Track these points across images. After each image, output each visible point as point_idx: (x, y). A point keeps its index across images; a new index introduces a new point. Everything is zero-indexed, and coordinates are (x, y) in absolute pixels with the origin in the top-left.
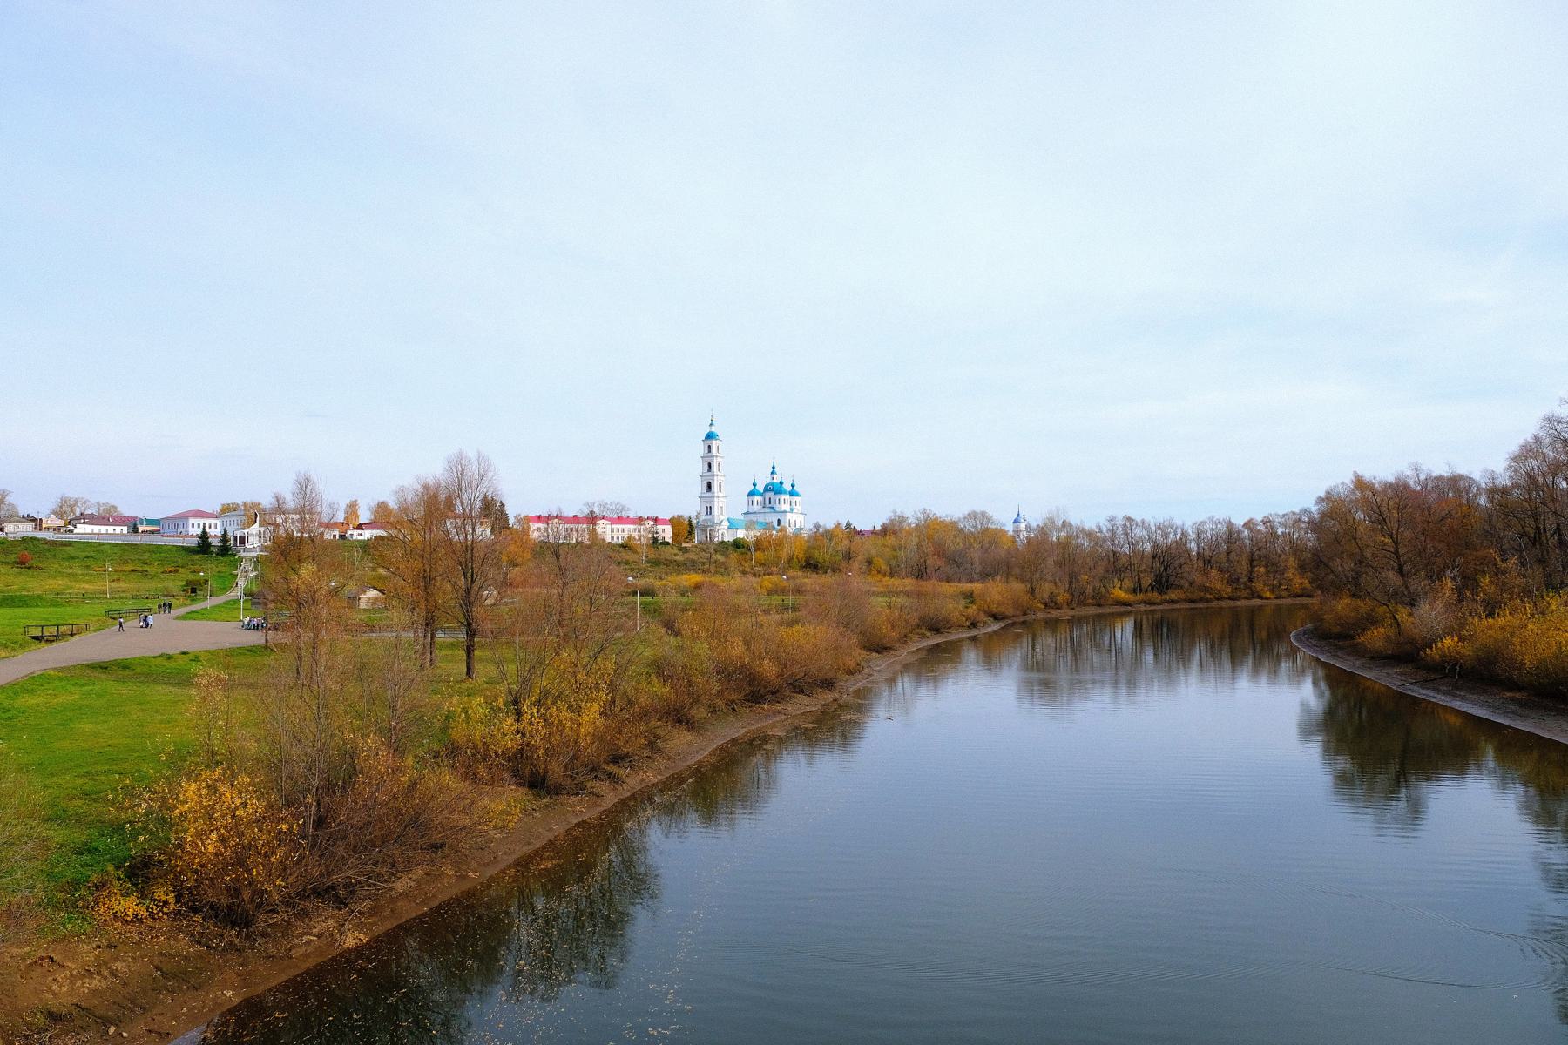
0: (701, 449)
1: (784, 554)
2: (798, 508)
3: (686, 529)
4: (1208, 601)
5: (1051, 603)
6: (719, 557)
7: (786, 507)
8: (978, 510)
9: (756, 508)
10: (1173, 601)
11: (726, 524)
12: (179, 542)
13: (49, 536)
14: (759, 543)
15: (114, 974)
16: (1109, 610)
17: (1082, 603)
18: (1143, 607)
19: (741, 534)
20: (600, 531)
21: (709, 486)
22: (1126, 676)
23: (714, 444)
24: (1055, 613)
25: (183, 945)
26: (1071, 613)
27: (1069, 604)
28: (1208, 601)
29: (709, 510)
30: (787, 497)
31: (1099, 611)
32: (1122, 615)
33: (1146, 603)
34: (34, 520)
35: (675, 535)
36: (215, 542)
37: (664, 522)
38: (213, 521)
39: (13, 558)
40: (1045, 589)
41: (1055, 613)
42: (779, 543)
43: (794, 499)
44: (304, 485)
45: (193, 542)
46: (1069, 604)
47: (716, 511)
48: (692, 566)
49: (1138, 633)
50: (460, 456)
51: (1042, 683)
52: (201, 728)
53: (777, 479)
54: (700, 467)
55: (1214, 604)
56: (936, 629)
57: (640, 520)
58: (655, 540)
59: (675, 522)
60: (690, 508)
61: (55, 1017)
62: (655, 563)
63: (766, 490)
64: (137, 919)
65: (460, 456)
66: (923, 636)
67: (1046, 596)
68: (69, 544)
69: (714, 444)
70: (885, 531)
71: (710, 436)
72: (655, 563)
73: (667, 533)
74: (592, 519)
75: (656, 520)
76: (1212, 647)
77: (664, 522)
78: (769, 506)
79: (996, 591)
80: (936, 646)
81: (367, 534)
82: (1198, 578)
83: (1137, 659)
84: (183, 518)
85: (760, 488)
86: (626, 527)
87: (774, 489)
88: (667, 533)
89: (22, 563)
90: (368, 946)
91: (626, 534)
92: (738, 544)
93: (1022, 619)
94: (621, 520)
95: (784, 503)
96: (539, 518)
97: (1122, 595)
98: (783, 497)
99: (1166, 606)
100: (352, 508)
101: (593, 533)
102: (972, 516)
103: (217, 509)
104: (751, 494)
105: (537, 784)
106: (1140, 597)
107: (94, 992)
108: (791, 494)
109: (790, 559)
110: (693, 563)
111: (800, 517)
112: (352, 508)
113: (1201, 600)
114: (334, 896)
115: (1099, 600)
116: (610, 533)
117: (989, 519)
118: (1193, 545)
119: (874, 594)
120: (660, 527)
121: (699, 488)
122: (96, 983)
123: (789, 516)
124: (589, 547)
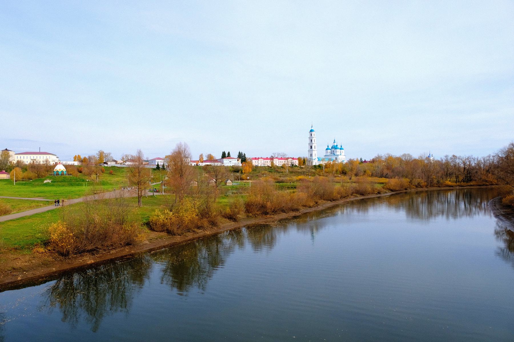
0: (308, 135)
1: (335, 169)
2: (343, 154)
3: (303, 161)
4: (486, 185)
5: (418, 185)
6: (313, 170)
7: (338, 153)
8: (406, 153)
9: (328, 154)
10: (471, 185)
11: (317, 159)
12: (152, 167)
13: (119, 165)
14: (326, 166)
15: (32, 263)
16: (442, 188)
17: (433, 186)
18: (458, 188)
19: (321, 163)
20: (274, 162)
21: (311, 147)
22: (453, 212)
23: (313, 133)
24: (420, 189)
25: (50, 259)
26: (426, 189)
27: (426, 186)
28: (486, 185)
29: (311, 155)
30: (339, 150)
31: (439, 189)
32: (450, 190)
33: (459, 186)
34: (115, 161)
35: (300, 163)
36: (161, 167)
37: (296, 159)
38: (161, 161)
39: (109, 172)
40: (416, 181)
41: (420, 189)
42: (333, 166)
43: (342, 151)
44: (140, 152)
45: (155, 167)
46: (426, 186)
47: (313, 155)
48: (303, 173)
49: (457, 197)
50: (180, 144)
51: (413, 211)
52: (38, 215)
53: (335, 144)
54: (308, 141)
55: (489, 187)
56: (362, 194)
57: (287, 159)
58: (293, 165)
59: (299, 159)
60: (305, 155)
61: (14, 269)
62: (291, 172)
63: (332, 148)
64: (42, 253)
65: (180, 144)
66: (356, 196)
67: (416, 184)
68: (123, 168)
69: (313, 133)
70: (373, 161)
71: (311, 131)
72: (291, 172)
73: (296, 163)
74: (272, 159)
75: (293, 159)
76: (409, 205)
77: (296, 159)
78: (333, 153)
79: (393, 182)
80: (363, 199)
81: (204, 164)
82: (484, 177)
83: (457, 205)
84: (154, 160)
85: (330, 147)
86: (283, 161)
87: (335, 147)
88: (296, 163)
89: (111, 173)
90: (94, 263)
91: (283, 163)
92: (320, 166)
93: (405, 191)
94: (281, 159)
95: (338, 152)
96: (256, 159)
97: (450, 183)
98: (337, 150)
99: (468, 187)
100: (201, 156)
101: (272, 163)
102: (404, 155)
103: (164, 157)
104: (327, 149)
105: (169, 232)
106: (458, 184)
107: (25, 266)
108: (341, 149)
109: (337, 171)
110: (304, 172)
111: (343, 158)
112: (201, 156)
113: (483, 185)
114: (92, 252)
115: (439, 184)
116: (278, 163)
117: (411, 156)
118: (482, 166)
119: (376, 183)
120: (294, 161)
121: (308, 148)
122: (26, 264)
123: (339, 156)
124: (271, 167)
